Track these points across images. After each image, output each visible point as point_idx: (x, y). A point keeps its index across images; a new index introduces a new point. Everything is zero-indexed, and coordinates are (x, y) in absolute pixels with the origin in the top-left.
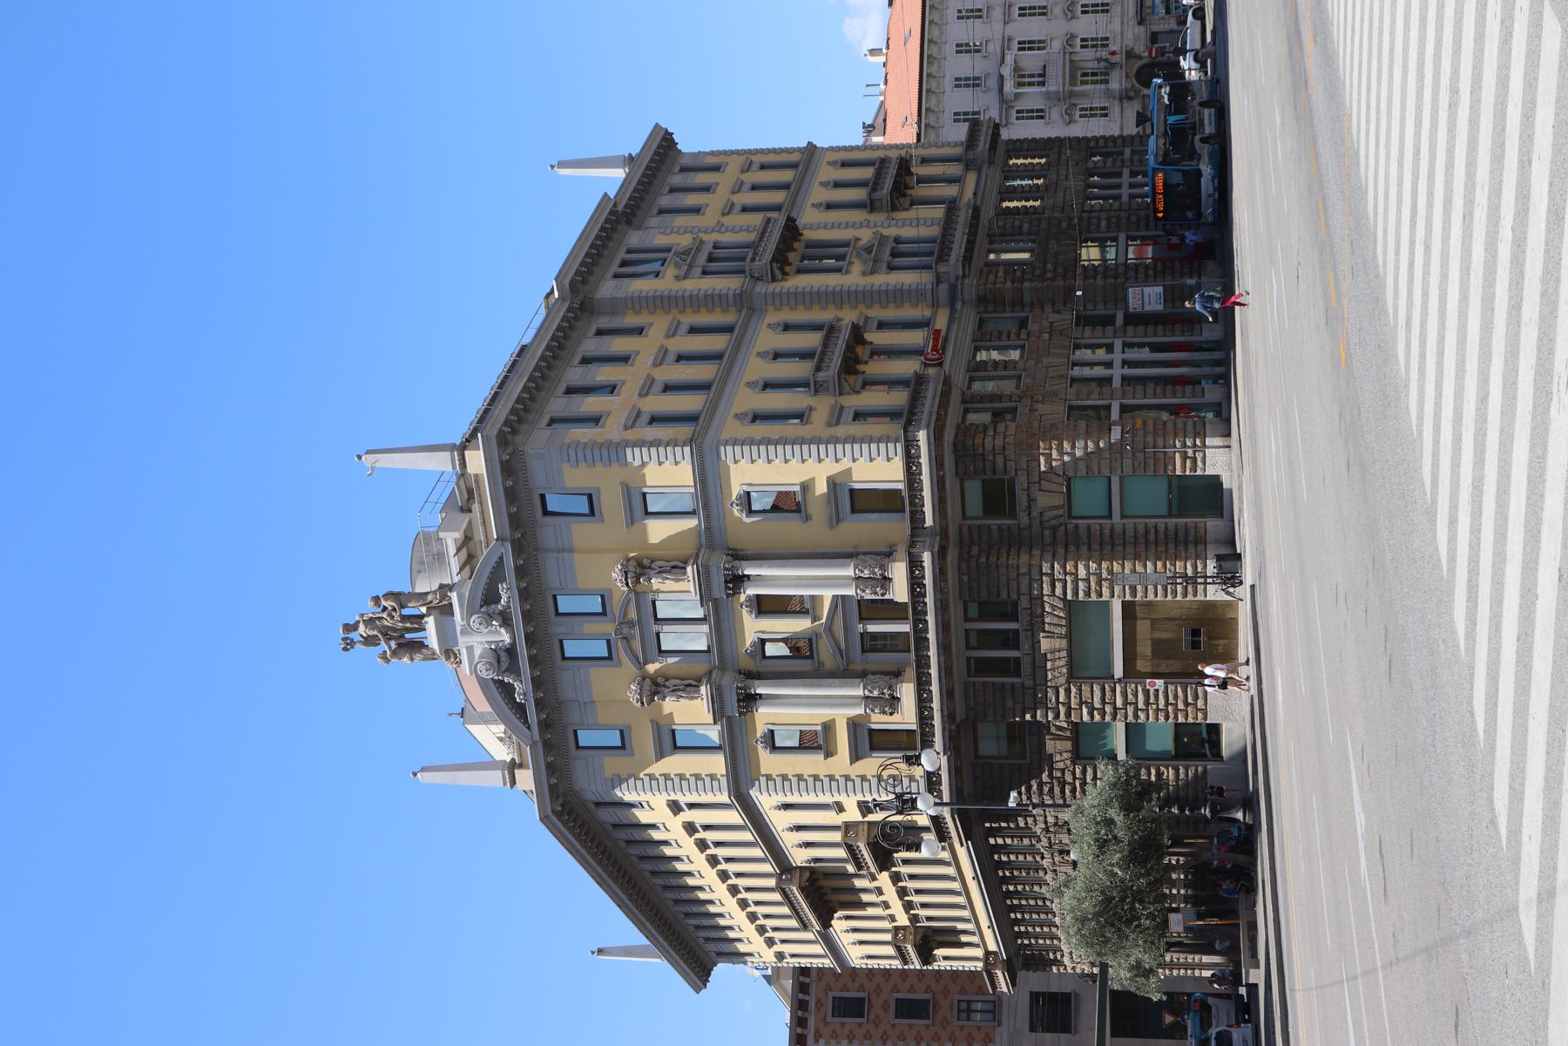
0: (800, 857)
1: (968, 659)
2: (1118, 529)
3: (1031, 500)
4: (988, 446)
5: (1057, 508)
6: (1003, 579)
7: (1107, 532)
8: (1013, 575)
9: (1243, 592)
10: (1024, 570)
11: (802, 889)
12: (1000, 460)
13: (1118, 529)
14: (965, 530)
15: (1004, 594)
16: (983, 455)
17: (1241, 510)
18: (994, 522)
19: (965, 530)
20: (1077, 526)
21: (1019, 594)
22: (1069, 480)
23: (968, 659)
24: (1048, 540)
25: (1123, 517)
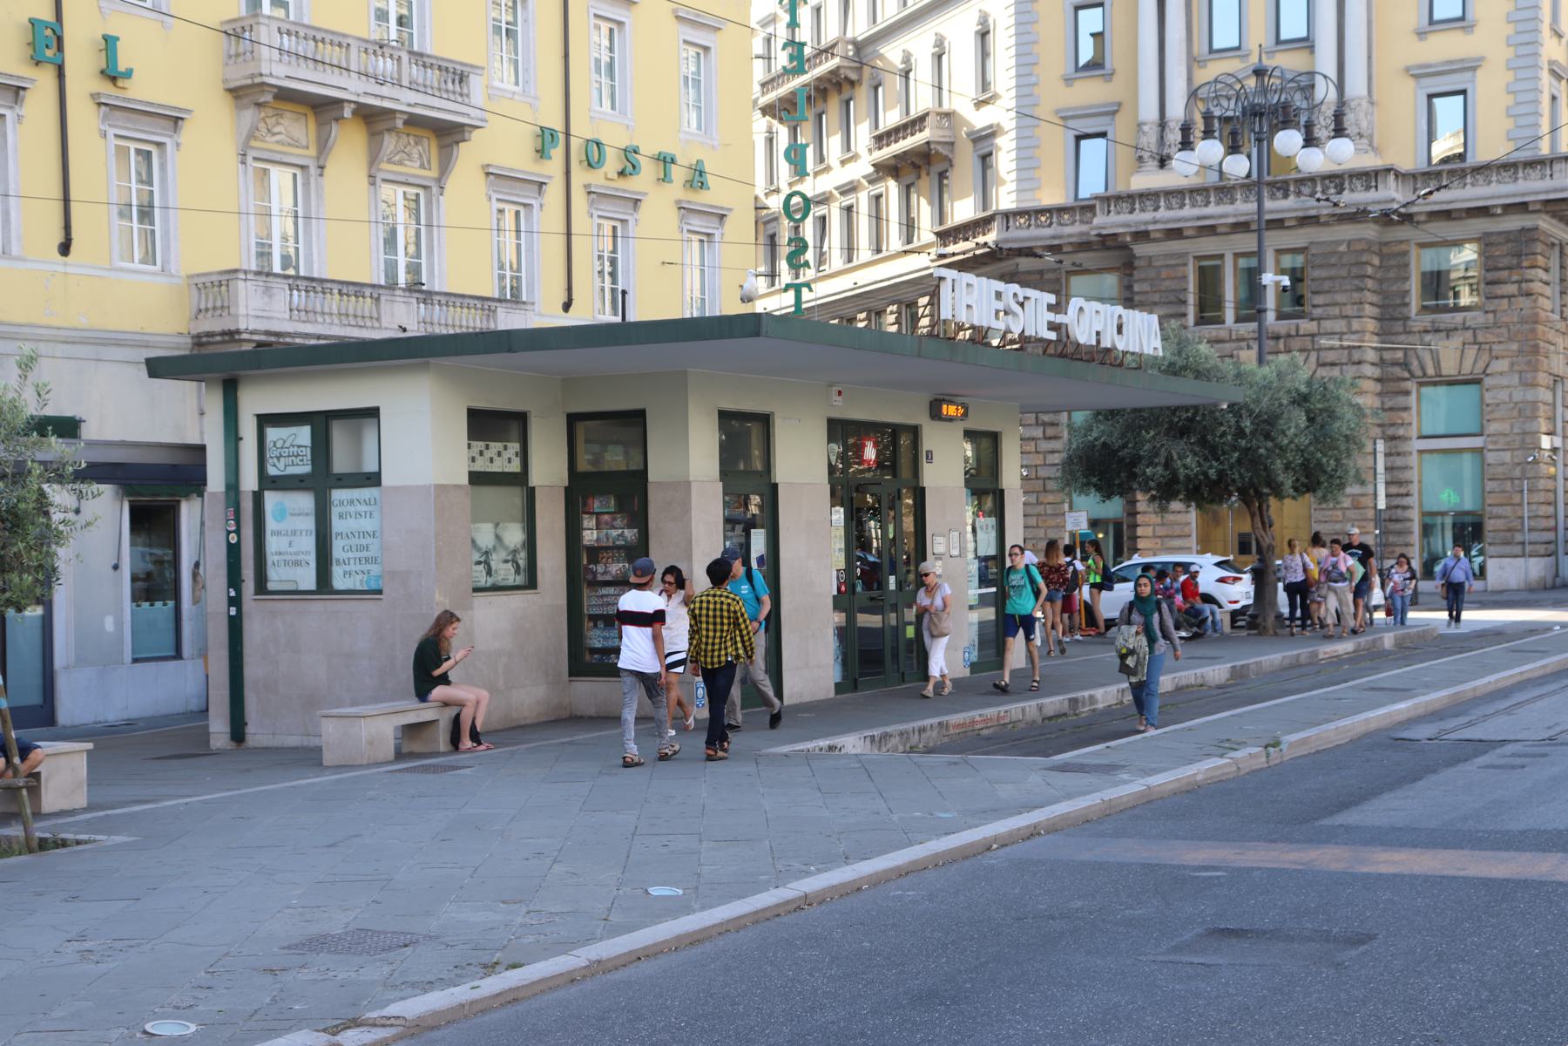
0: (892, 52)
1: (1221, 256)
2: (1404, 447)
3: (1449, 332)
4: (1531, 273)
5: (1437, 364)
6: (1340, 298)
7: (1401, 432)
8: (1349, 310)
9: (137, 266)
10: (1356, 325)
11: (834, 72)
12: (1511, 289)
13: (1404, 447)
14: (1403, 247)
15: (1318, 300)
16: (1519, 266)
17: (319, 337)
18: (1414, 285)
19: (1403, 247)
20: (1407, 393)
21: (1319, 319)
22: (1477, 382)
23: (1221, 256)
24: (1387, 356)
25: (1421, 452)
